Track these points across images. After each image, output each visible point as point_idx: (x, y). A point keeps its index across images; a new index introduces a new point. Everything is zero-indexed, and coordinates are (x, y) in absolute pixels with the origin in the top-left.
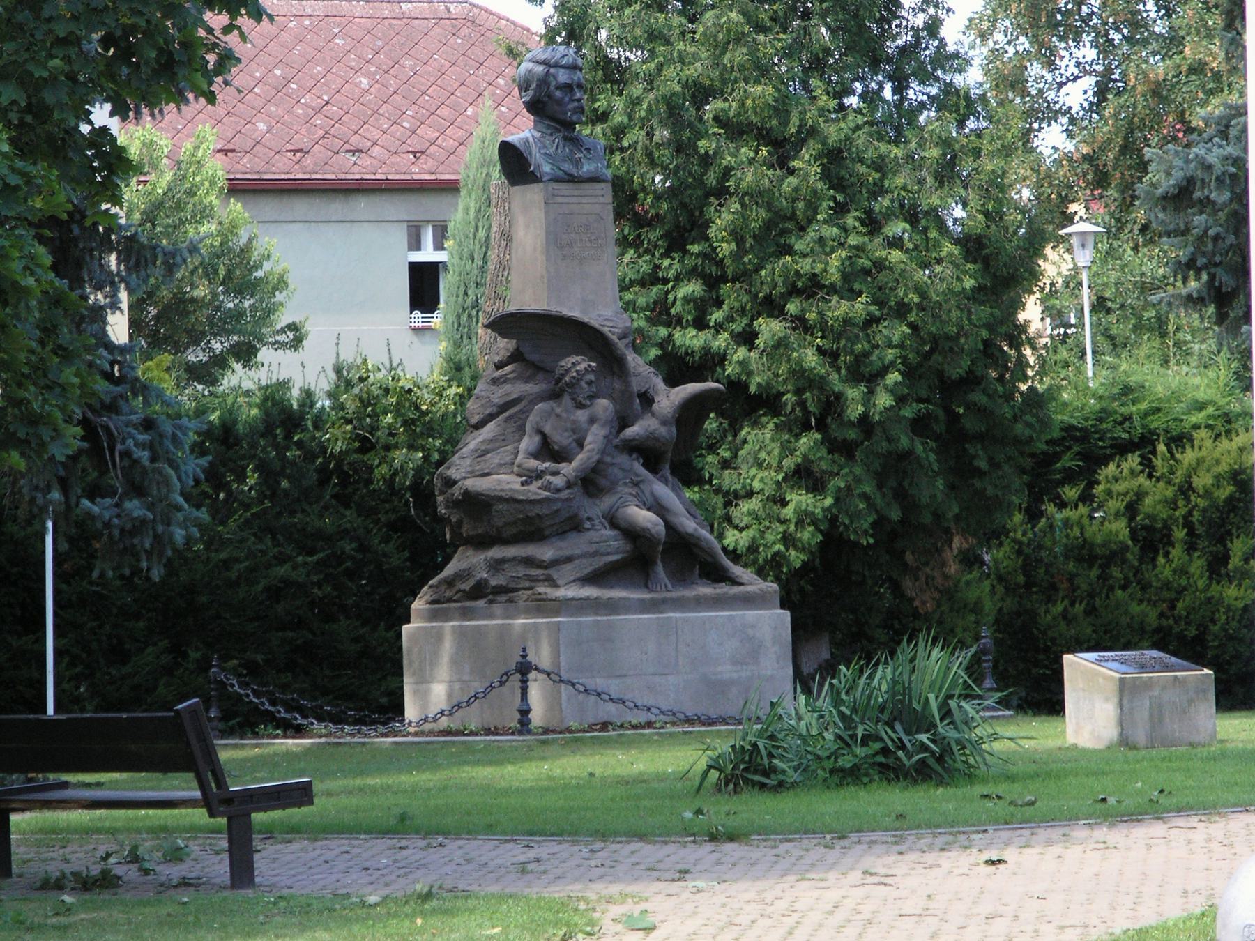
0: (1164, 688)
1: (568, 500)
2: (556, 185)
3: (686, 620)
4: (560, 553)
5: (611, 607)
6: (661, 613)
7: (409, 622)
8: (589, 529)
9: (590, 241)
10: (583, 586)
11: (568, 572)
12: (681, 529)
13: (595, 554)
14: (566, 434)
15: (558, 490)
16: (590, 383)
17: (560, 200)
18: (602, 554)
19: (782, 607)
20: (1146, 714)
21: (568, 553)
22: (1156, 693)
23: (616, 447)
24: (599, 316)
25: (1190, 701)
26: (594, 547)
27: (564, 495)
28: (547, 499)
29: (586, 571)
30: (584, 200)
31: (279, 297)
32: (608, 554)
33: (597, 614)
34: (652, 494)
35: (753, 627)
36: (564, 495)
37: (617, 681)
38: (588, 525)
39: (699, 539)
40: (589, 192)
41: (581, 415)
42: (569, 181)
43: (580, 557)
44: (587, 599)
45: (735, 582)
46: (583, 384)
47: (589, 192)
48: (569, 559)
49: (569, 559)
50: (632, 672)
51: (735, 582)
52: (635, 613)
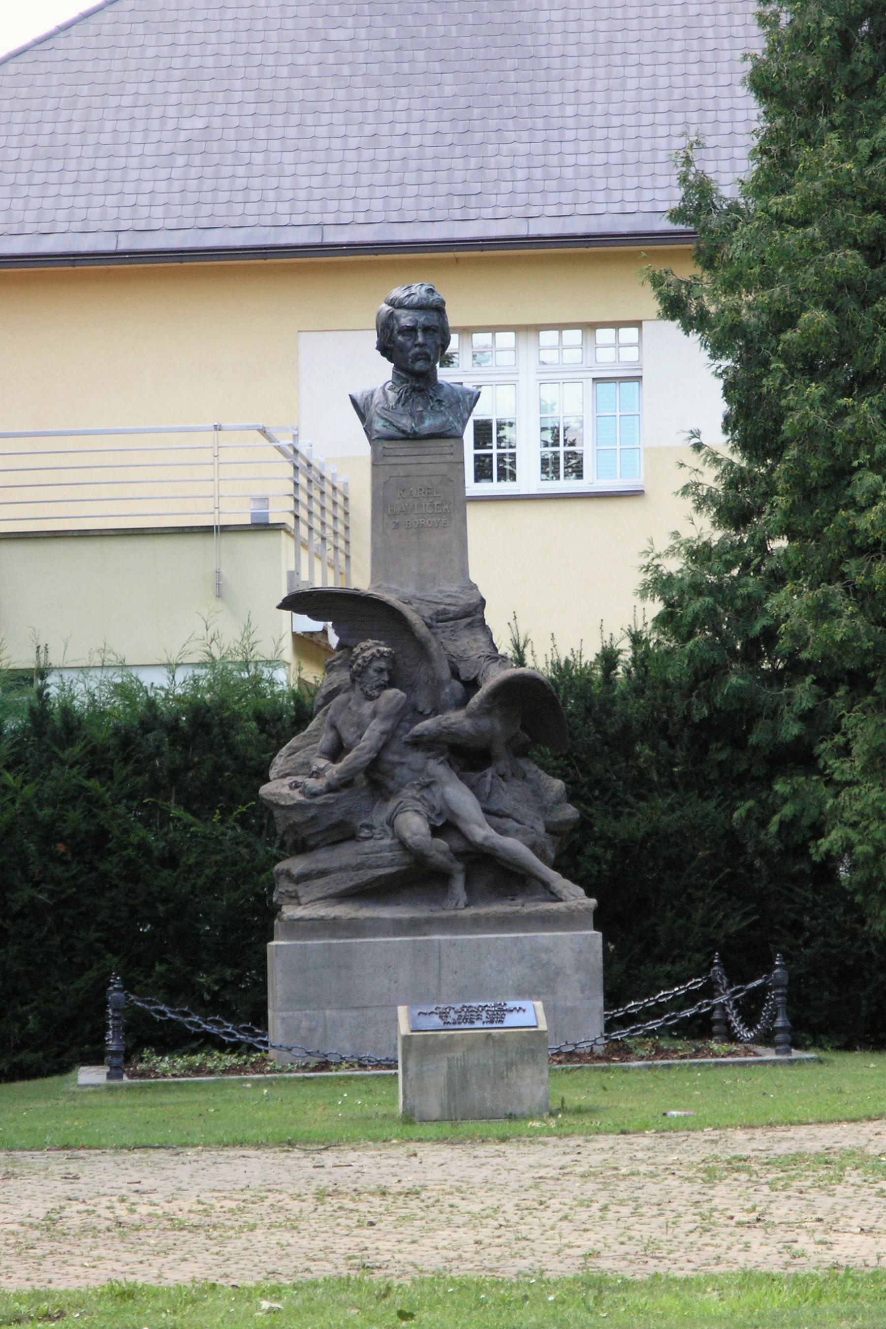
0: (470, 1049)
1: (324, 805)
2: (387, 444)
3: (453, 944)
4: (313, 866)
5: (354, 928)
6: (425, 935)
7: (272, 939)
8: (367, 839)
9: (432, 506)
10: (340, 903)
11: (318, 887)
12: (470, 838)
13: (359, 867)
14: (352, 730)
15: (315, 795)
16: (380, 671)
17: (393, 460)
18: (371, 867)
19: (596, 928)
20: (442, 1080)
21: (321, 866)
22: (459, 1054)
23: (406, 743)
24: (441, 592)
25: (510, 1065)
26: (359, 859)
27: (319, 800)
28: (299, 806)
29: (343, 887)
30: (425, 460)
31: (674, 565)
32: (379, 867)
33: (333, 936)
34: (443, 797)
35: (548, 950)
36: (319, 800)
37: (355, 1013)
38: (365, 833)
39: (493, 849)
40: (433, 450)
41: (367, 708)
42: (402, 439)
43: (340, 869)
44: (322, 919)
45: (555, 897)
46: (371, 672)
47: (433, 450)
48: (323, 873)
49: (323, 873)
50: (376, 1003)
51: (555, 897)
52: (387, 934)
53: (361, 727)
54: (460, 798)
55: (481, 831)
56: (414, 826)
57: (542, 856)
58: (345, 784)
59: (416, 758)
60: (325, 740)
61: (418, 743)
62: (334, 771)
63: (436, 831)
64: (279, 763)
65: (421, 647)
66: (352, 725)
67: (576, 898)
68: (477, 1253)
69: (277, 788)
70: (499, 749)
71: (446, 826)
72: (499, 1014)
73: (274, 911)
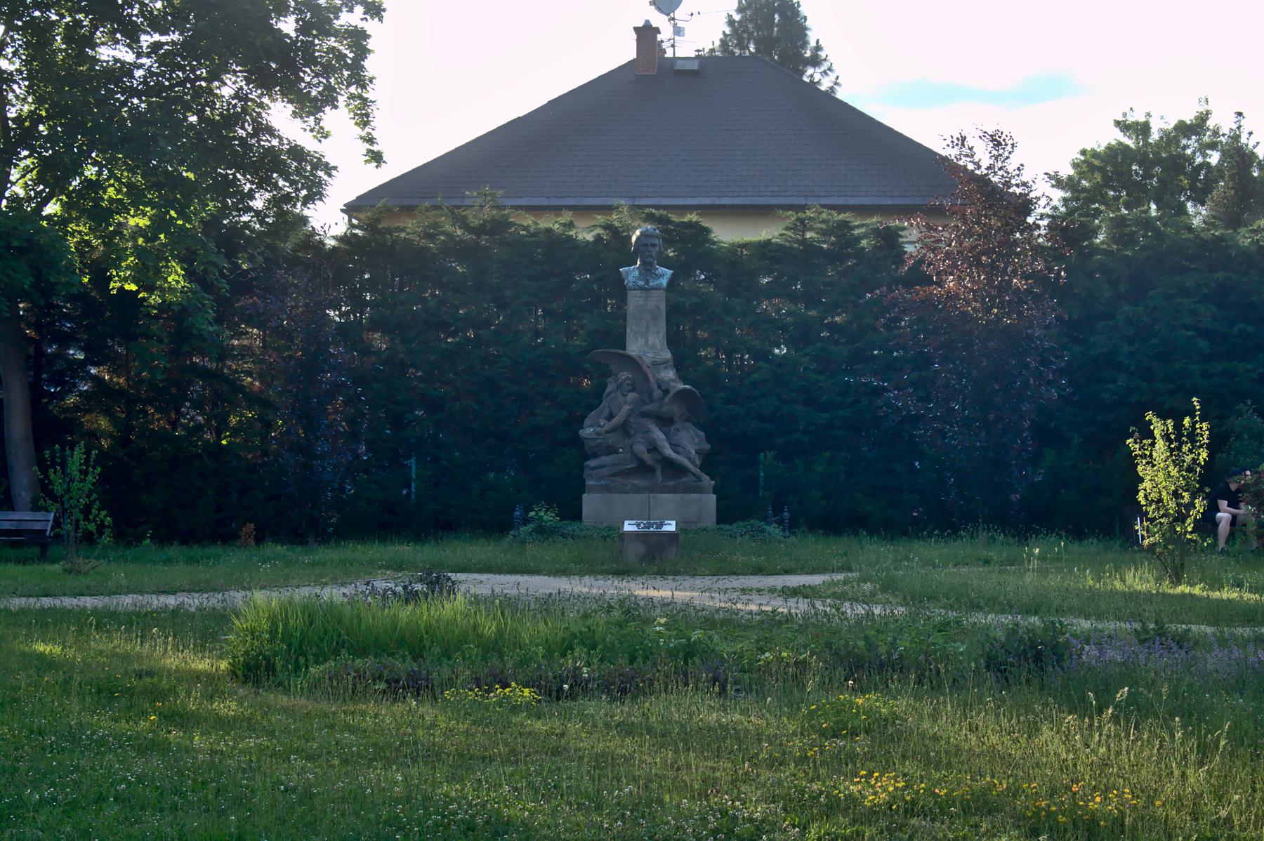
53: (620, 407)
54: (658, 435)
55: (669, 452)
56: (641, 449)
57: (693, 463)
58: (613, 430)
59: (643, 421)
60: (606, 412)
61: (644, 415)
62: (608, 426)
63: (649, 451)
64: (587, 421)
65: (646, 376)
66: (187, 249)
67: (707, 481)
68: (327, 440)
69: (587, 432)
70: (676, 418)
71: (654, 449)
72: (662, 525)
73: (584, 486)
